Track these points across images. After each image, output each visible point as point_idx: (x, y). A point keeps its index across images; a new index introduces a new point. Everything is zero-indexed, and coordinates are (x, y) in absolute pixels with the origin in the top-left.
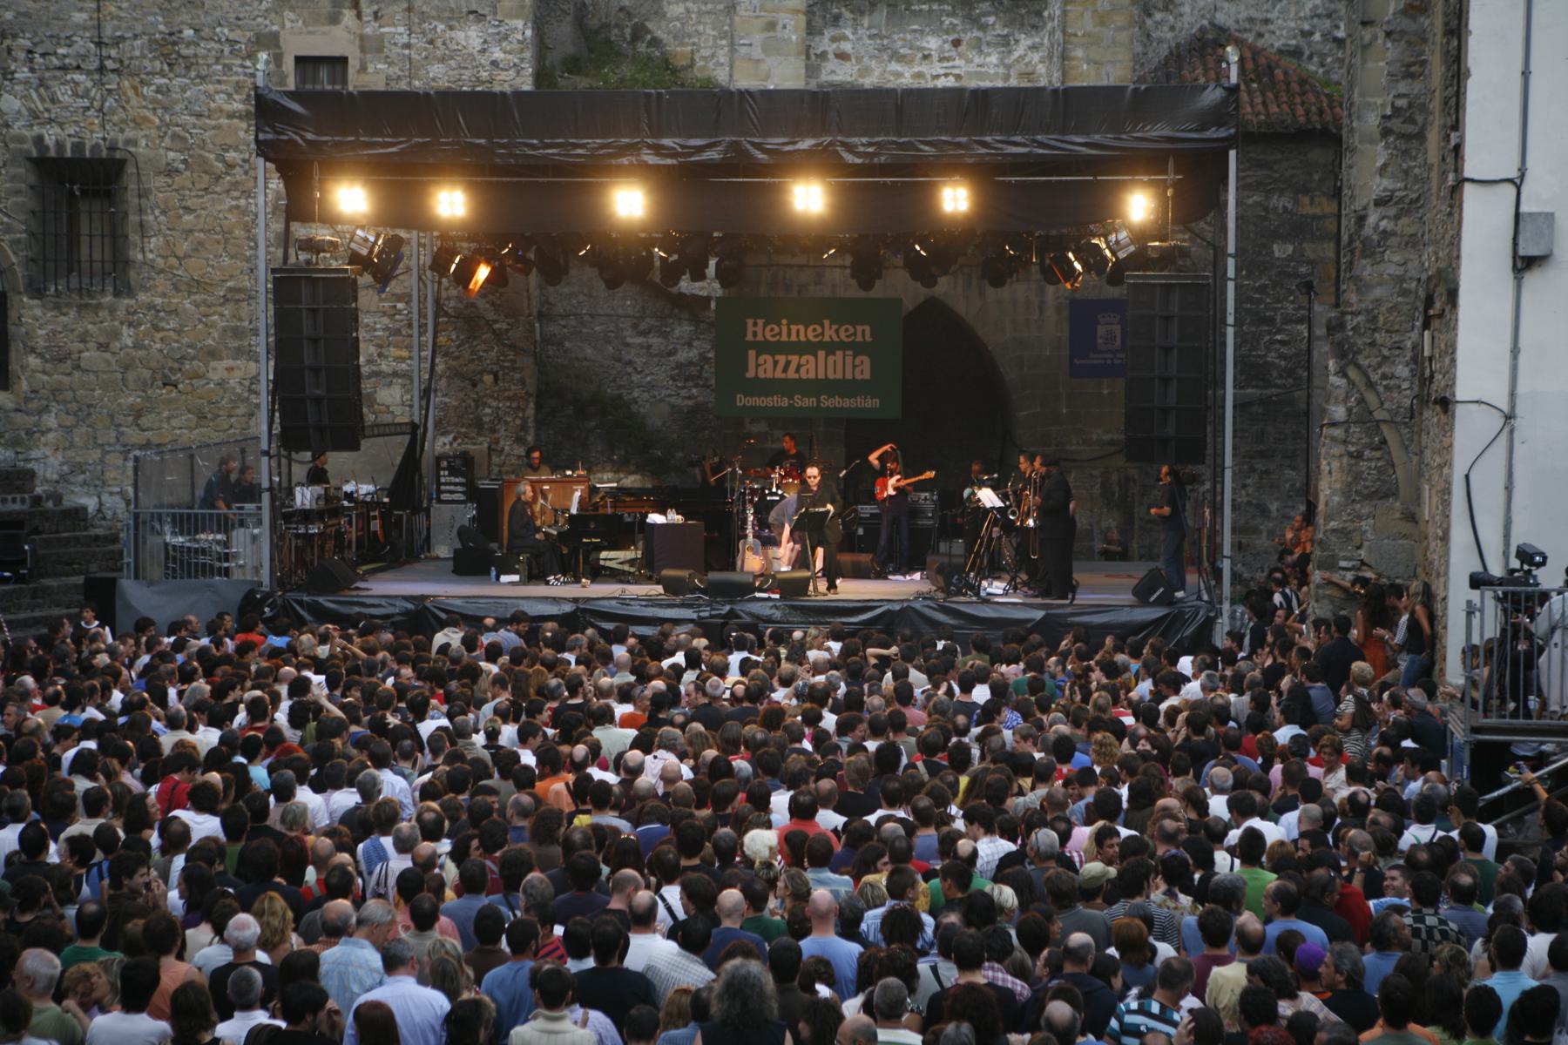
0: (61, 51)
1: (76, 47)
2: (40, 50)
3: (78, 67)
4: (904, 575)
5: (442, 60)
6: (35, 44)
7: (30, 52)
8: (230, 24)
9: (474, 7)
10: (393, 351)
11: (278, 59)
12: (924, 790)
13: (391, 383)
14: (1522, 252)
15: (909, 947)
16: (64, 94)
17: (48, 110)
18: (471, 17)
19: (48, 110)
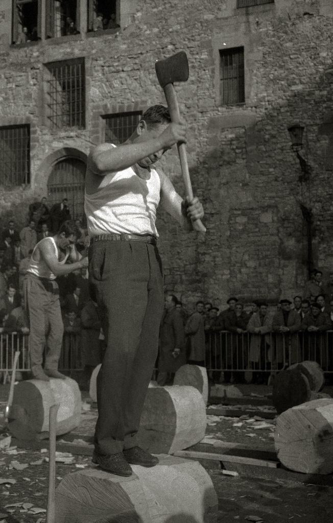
0: (116, 64)
1: (121, 61)
2: (107, 64)
3: (123, 71)
4: (63, 452)
5: (291, 41)
6: (105, 63)
7: (103, 66)
8: (189, 39)
9: (307, 11)
10: (268, 194)
11: (210, 53)
12: (197, 257)
13: (267, 211)
14: (211, 395)
15: (243, 182)
16: (116, 84)
17: (109, 92)
18: (306, 16)
19: (109, 92)
